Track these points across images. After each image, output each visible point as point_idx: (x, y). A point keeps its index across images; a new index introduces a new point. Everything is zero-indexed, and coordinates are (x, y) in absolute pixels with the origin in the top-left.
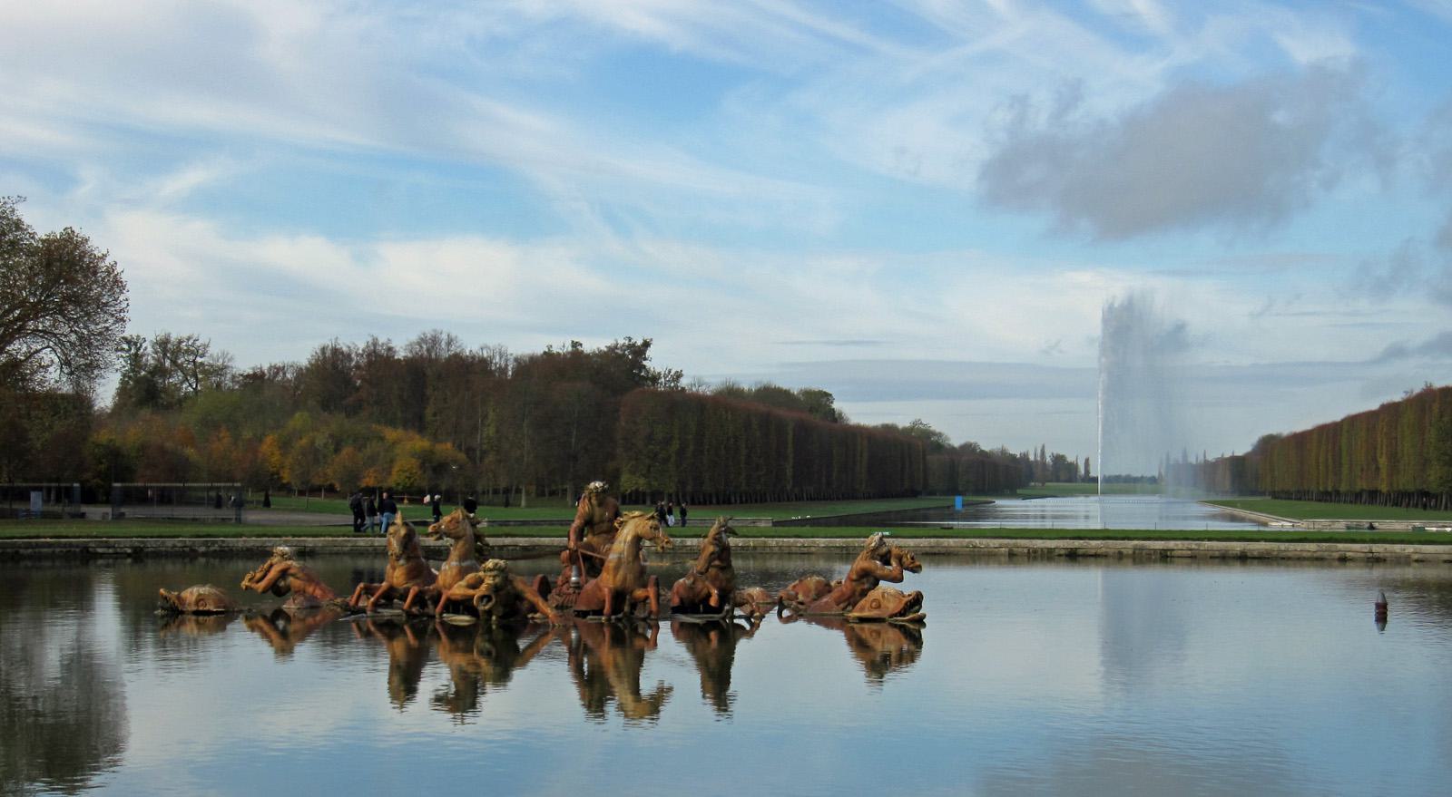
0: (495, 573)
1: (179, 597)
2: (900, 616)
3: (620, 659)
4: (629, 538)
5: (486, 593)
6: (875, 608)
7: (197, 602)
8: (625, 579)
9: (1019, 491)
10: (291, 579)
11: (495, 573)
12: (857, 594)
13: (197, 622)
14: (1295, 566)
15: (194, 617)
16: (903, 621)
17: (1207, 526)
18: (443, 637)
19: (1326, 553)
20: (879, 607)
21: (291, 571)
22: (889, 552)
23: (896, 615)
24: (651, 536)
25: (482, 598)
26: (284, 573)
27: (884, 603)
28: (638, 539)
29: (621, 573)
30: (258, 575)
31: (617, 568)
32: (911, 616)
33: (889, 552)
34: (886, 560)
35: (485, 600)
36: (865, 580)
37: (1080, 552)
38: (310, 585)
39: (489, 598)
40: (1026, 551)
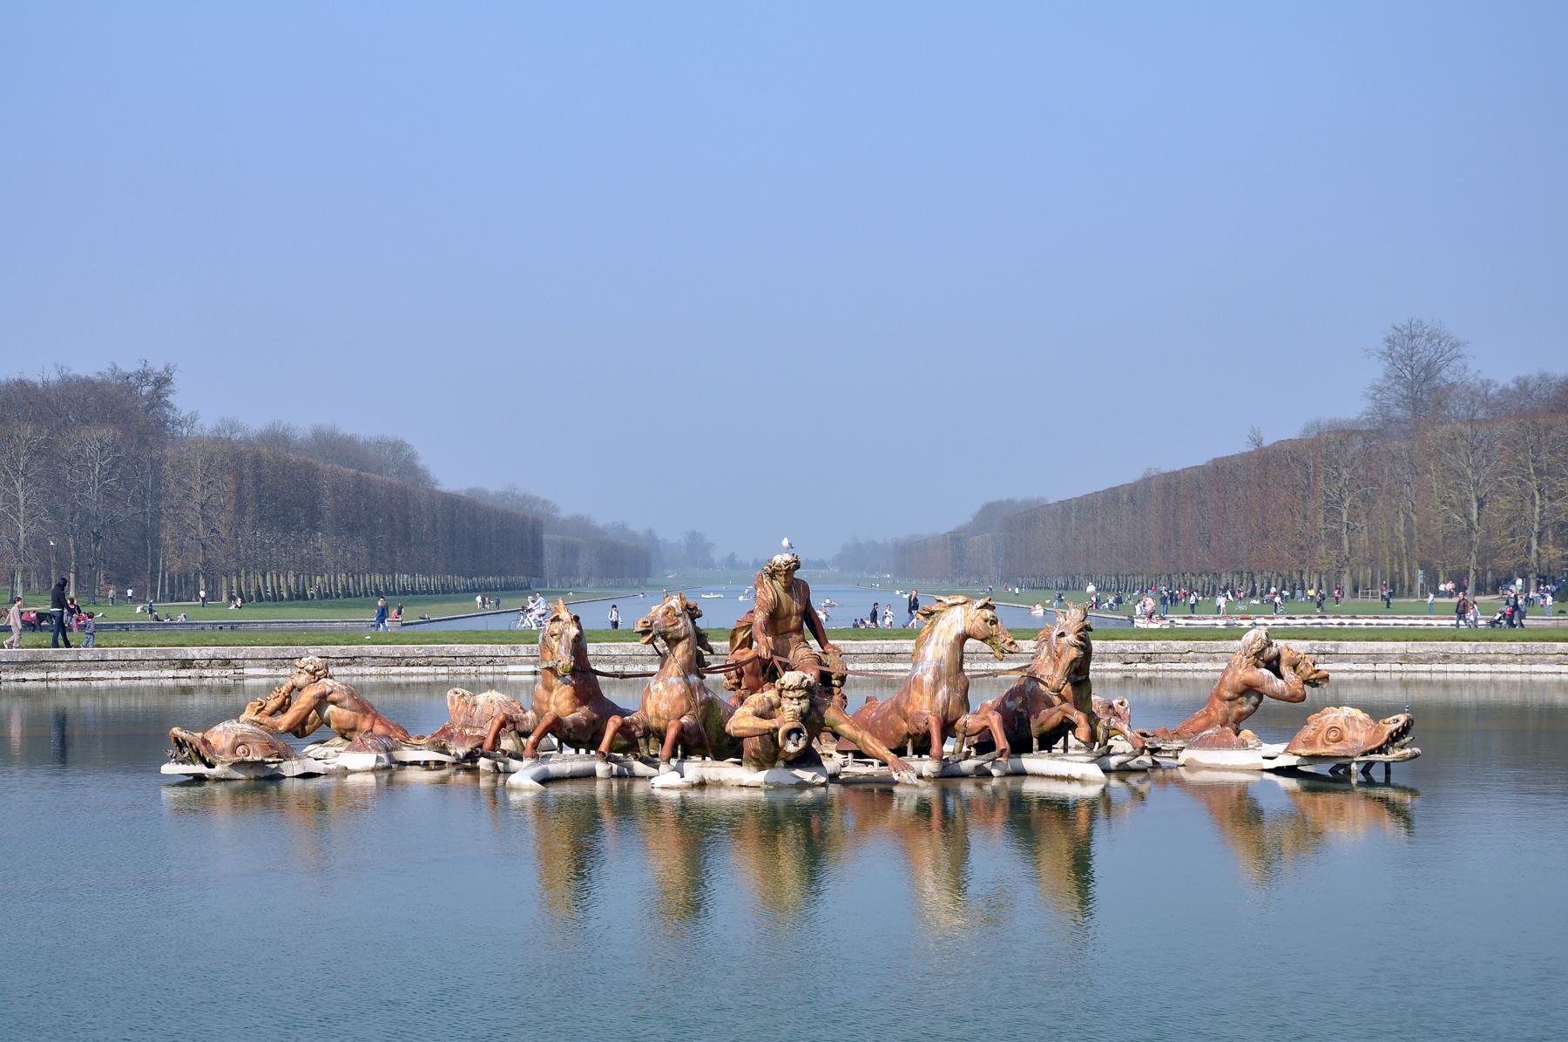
0: (801, 693)
1: (205, 742)
4: (951, 637)
5: (796, 724)
8: (946, 705)
9: (650, 581)
10: (331, 708)
11: (801, 693)
20: (1340, 739)
21: (334, 696)
23: (1372, 752)
25: (788, 734)
26: (322, 701)
27: (1349, 734)
28: (964, 637)
30: (272, 704)
31: (935, 686)
33: (1278, 657)
34: (1273, 665)
35: (794, 736)
39: (798, 731)
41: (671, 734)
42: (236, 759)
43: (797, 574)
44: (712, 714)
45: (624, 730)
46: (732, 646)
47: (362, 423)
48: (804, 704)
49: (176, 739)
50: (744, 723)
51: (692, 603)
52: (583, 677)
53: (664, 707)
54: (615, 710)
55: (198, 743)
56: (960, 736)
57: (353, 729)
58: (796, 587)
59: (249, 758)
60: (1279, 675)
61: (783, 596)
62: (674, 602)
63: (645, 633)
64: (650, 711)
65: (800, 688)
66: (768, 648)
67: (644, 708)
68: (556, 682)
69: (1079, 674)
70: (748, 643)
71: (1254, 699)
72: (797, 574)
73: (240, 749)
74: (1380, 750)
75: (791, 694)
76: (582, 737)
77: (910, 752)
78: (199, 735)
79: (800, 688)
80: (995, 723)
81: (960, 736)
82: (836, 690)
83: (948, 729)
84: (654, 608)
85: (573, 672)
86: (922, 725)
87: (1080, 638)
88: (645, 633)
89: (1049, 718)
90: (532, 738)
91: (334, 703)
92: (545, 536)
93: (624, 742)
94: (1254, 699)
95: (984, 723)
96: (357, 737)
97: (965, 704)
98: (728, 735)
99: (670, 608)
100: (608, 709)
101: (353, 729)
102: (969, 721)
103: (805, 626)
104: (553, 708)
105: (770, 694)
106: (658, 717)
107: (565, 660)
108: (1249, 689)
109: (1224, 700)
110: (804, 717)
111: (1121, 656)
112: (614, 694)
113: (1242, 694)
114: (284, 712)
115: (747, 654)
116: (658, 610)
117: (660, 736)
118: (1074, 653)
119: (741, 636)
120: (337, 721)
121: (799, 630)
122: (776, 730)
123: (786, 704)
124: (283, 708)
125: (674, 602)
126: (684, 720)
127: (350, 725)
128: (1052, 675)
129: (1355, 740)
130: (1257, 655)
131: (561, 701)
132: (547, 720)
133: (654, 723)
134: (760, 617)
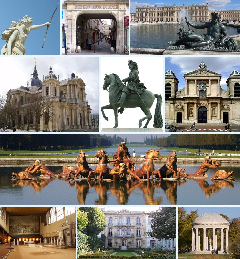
0: (123, 167)
1: (18, 175)
2: (228, 178)
3: (149, 191)
5: (122, 173)
6: (220, 176)
7: (23, 176)
10: (41, 169)
12: (203, 172)
13: (23, 182)
14: (227, 54)
15: (22, 181)
16: (229, 180)
17: (230, 120)
18: (100, 185)
19: (181, 161)
21: (42, 167)
22: (211, 161)
23: (226, 178)
24: (157, 157)
25: (120, 174)
26: (39, 168)
27: (223, 175)
28: (153, 157)
29: (149, 167)
32: (231, 178)
33: (211, 161)
34: (211, 163)
35: (121, 175)
36: (205, 169)
37: (197, 161)
38: (47, 171)
40: (183, 161)
41: (100, 174)
42: (23, 178)
43: (125, 146)
44: (108, 170)
45: (92, 173)
46: (114, 158)
47: (118, 75)
48: (124, 169)
49: (13, 175)
50: (113, 172)
51: (105, 151)
52: (85, 164)
53: (100, 169)
54: (90, 170)
55: (17, 175)
56: (152, 175)
57: (45, 173)
58: (125, 148)
59: (25, 178)
60: (212, 165)
61: (123, 150)
62: (102, 151)
63: (96, 156)
64: (97, 170)
65: (123, 166)
66: (120, 159)
67: (96, 169)
68: (80, 165)
69: (174, 164)
70: (116, 158)
71: (207, 168)
72: (125, 146)
73: (24, 176)
74: (228, 178)
75: (121, 167)
76: (85, 175)
77: (144, 178)
78: (17, 174)
79: (123, 166)
80: (159, 172)
81: (152, 175)
82: (132, 167)
83: (150, 173)
84: (98, 152)
85: (83, 163)
86: (145, 173)
87: (174, 157)
88: (96, 156)
89: (168, 172)
90: (76, 175)
91: (42, 168)
92: (91, 138)
93: (92, 176)
94: (207, 168)
95: (157, 173)
96: (45, 174)
97: (154, 169)
98: (110, 174)
99: (101, 152)
100: (90, 169)
101: (45, 173)
102: (154, 172)
103: (127, 155)
104: (80, 170)
105: (118, 167)
106: (98, 171)
107: (82, 161)
108: (206, 167)
109: (202, 169)
110: (123, 171)
111: (184, 162)
112: (91, 166)
113: (205, 168)
114: (33, 170)
115: (116, 160)
116: (98, 152)
117: (99, 174)
118: (173, 160)
119: (115, 157)
120: (42, 172)
121: (126, 156)
122: (118, 173)
123: (120, 169)
124: (32, 169)
125: (102, 151)
126: (103, 172)
127: (44, 172)
128: (169, 165)
129: (223, 176)
130: (208, 161)
131: (81, 168)
132: (79, 171)
133: (98, 172)
134: (119, 153)
